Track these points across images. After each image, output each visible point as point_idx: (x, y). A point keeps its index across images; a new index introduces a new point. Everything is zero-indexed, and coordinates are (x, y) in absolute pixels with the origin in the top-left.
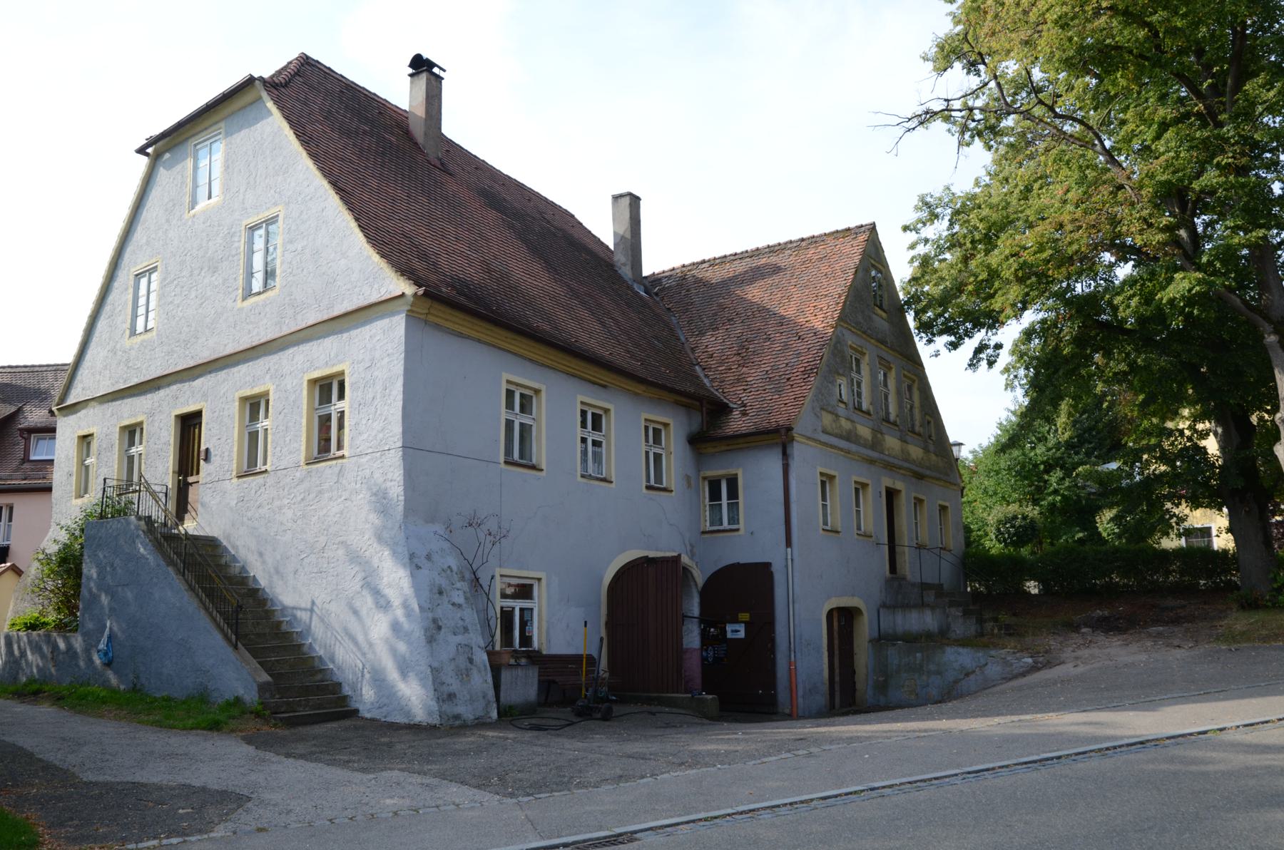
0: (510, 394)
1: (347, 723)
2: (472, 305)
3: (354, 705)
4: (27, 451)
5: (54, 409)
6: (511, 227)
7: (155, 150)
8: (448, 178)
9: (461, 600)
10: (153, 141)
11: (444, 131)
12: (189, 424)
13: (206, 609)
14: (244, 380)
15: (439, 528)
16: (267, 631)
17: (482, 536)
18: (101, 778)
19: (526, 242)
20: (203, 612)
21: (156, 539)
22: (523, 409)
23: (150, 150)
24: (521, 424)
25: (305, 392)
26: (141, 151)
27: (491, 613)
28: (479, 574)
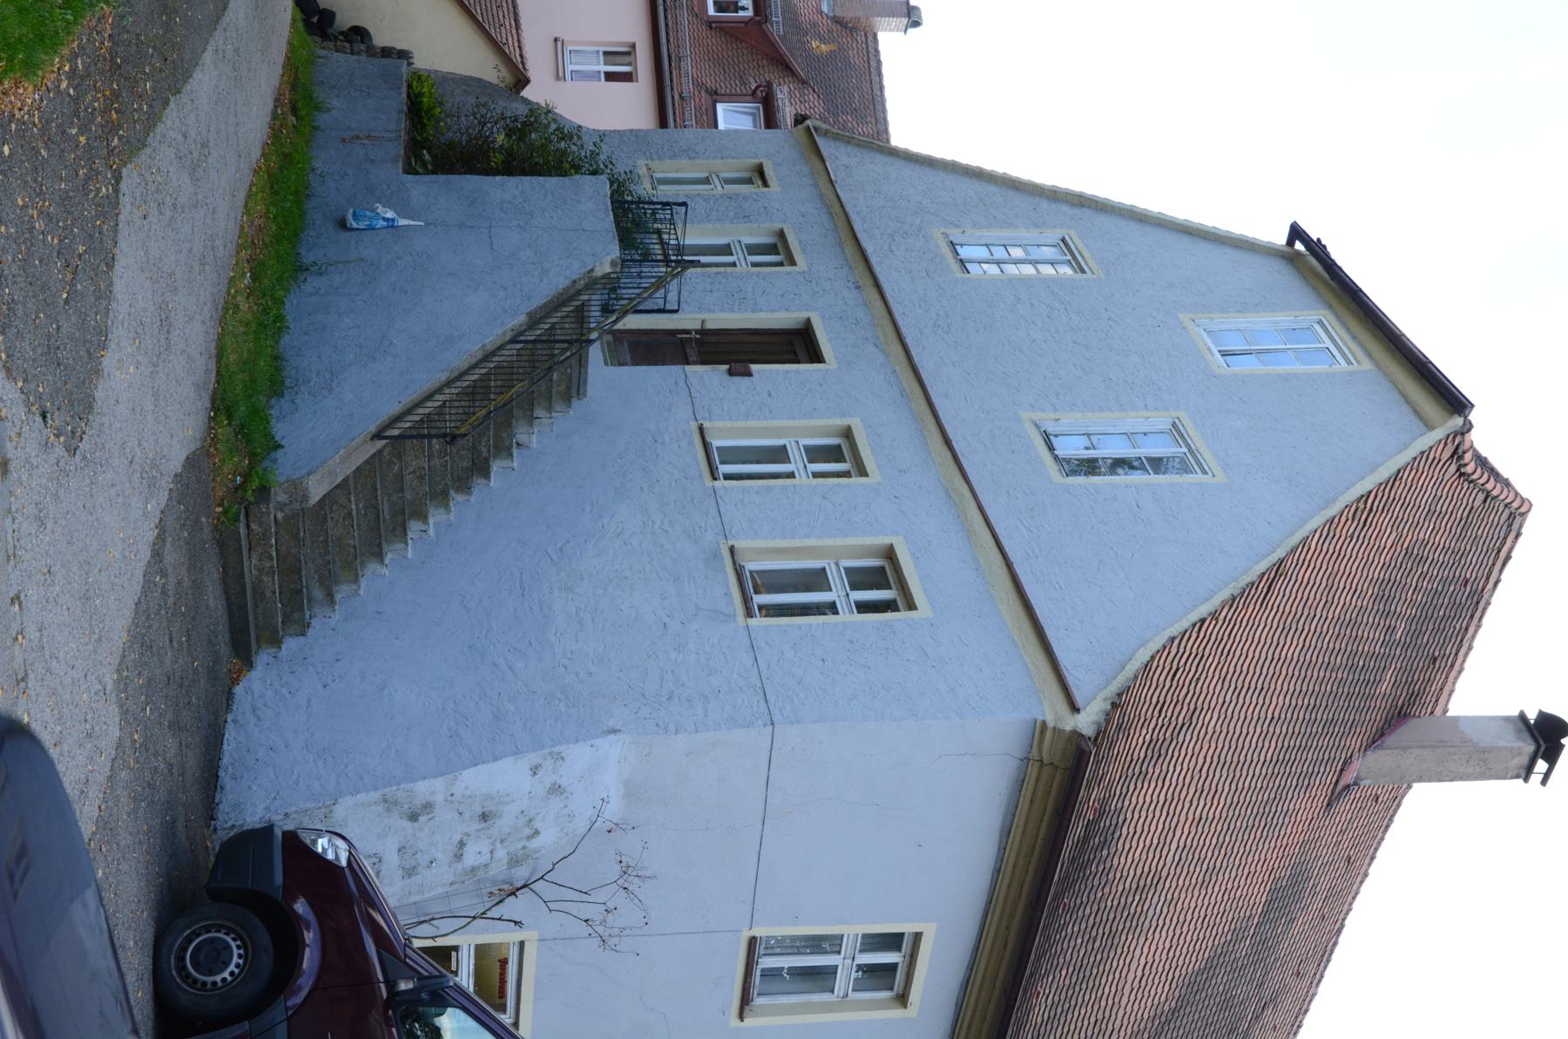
0: (892, 941)
1: (224, 648)
2: (1065, 854)
3: (262, 658)
4: (730, 97)
5: (808, 122)
6: (1237, 936)
7: (1299, 253)
8: (1321, 802)
9: (471, 858)
10: (1317, 249)
11: (1415, 785)
12: (799, 345)
13: (448, 384)
14: (885, 432)
15: (614, 810)
16: (409, 495)
17: (600, 896)
18: (125, 200)
19: (1209, 967)
20: (443, 377)
21: (579, 293)
22: (870, 970)
23: (1299, 246)
24: (831, 971)
25: (868, 541)
26: (1296, 233)
27: (445, 925)
28: (524, 896)
